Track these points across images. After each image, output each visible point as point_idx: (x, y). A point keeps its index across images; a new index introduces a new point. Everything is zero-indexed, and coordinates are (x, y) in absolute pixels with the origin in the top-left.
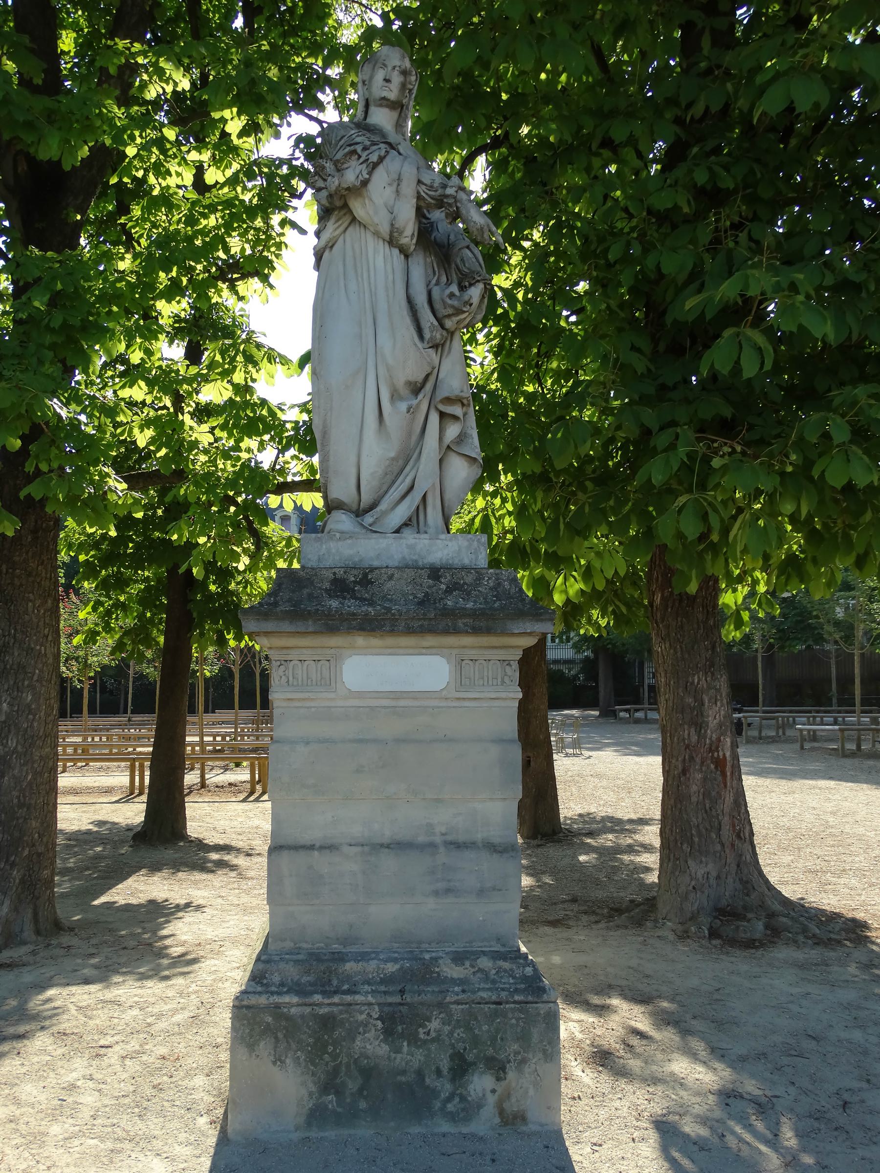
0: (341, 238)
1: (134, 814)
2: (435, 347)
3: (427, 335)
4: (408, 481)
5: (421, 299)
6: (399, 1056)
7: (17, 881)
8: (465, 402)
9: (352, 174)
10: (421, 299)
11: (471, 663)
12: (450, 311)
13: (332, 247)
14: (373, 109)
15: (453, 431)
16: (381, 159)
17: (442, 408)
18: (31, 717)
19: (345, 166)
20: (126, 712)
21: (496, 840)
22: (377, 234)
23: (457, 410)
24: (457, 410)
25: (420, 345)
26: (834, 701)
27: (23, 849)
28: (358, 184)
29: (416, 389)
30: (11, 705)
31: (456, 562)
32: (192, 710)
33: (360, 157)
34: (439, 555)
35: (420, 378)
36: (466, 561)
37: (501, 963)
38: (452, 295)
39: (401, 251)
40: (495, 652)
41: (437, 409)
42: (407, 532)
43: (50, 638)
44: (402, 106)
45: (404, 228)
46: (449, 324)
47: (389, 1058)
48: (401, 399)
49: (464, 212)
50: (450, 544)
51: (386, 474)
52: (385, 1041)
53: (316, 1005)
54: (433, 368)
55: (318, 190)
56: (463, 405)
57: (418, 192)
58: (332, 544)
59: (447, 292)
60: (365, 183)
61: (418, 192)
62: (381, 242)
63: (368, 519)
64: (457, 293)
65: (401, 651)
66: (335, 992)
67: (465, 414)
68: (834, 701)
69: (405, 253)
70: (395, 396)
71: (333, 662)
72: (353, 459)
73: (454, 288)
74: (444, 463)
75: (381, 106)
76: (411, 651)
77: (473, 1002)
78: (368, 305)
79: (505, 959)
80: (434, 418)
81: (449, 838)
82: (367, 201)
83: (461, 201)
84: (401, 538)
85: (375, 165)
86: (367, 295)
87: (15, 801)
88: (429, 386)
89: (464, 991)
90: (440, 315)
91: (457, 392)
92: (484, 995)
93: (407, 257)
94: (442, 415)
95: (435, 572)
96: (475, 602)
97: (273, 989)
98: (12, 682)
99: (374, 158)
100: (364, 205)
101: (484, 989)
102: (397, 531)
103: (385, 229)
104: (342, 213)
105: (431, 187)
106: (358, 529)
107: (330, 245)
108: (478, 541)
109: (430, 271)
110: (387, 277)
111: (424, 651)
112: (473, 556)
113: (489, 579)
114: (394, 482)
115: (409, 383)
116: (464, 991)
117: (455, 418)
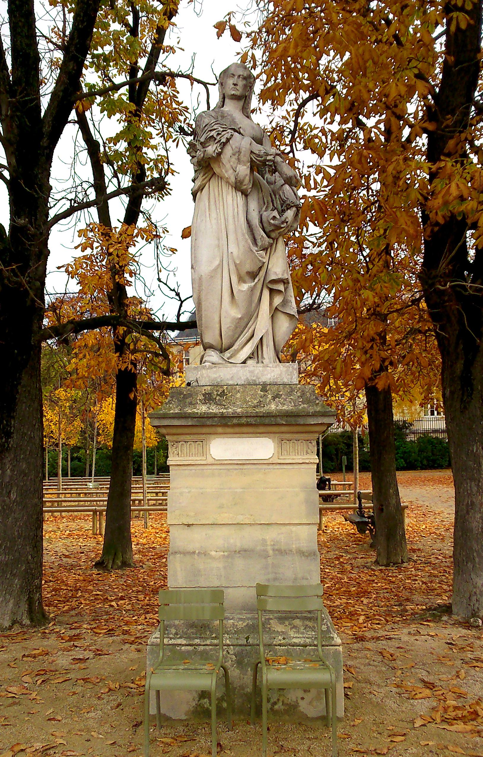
0: (207, 185)
1: (95, 545)
2: (265, 249)
3: (259, 244)
4: (251, 331)
5: (255, 221)
6: (245, 677)
7: (18, 586)
8: (286, 281)
9: (211, 149)
10: (255, 221)
11: (288, 442)
12: (272, 228)
13: (202, 189)
14: (227, 100)
15: (278, 300)
16: (228, 140)
17: (271, 286)
18: (25, 478)
19: (207, 145)
20: (90, 475)
21: (304, 549)
22: (228, 182)
23: (281, 287)
24: (281, 287)
25: (254, 249)
26: (69, 475)
27: (22, 566)
28: (215, 155)
29: (253, 275)
30: (12, 471)
31: (279, 381)
32: (138, 472)
33: (215, 139)
34: (269, 376)
35: (255, 269)
36: (285, 380)
37: (307, 623)
38: (274, 218)
39: (242, 193)
40: (302, 435)
41: (268, 288)
42: (250, 362)
43: (37, 426)
44: (246, 97)
45: (243, 180)
46: (273, 235)
47: (240, 678)
48: (245, 282)
49: (279, 169)
50: (275, 369)
51: (237, 327)
52: (237, 667)
53: (197, 645)
54: (264, 263)
55: (193, 157)
56: (284, 283)
57: (251, 158)
58: (204, 371)
59: (271, 216)
60: (219, 154)
61: (251, 158)
62: (230, 188)
63: (227, 354)
64: (278, 217)
65: (245, 435)
66: (208, 638)
67: (285, 289)
68: (69, 475)
69: (245, 194)
70: (241, 280)
71: (204, 442)
72: (217, 319)
73: (275, 213)
74: (274, 318)
75: (232, 99)
76: (251, 435)
77: (290, 645)
78: (223, 227)
79: (310, 621)
80: (266, 293)
81: (276, 547)
82: (221, 164)
83: (277, 163)
84: (245, 367)
85: (224, 144)
86: (223, 220)
87: (16, 533)
88: (262, 273)
89: (284, 639)
90: (267, 230)
91: (280, 276)
92: (295, 640)
93: (246, 196)
94: (271, 291)
95: (264, 387)
96: (288, 405)
97: (171, 636)
98: (13, 456)
99: (223, 140)
100: (219, 167)
101: (296, 637)
102: (244, 362)
103: (233, 180)
104: (207, 170)
105: (259, 156)
106: (221, 361)
107: (201, 189)
108: (292, 367)
109: (262, 203)
110: (234, 210)
111: (258, 435)
112: (289, 377)
113: (298, 391)
114: (242, 332)
115: (248, 273)
116: (284, 639)
117: (280, 292)
